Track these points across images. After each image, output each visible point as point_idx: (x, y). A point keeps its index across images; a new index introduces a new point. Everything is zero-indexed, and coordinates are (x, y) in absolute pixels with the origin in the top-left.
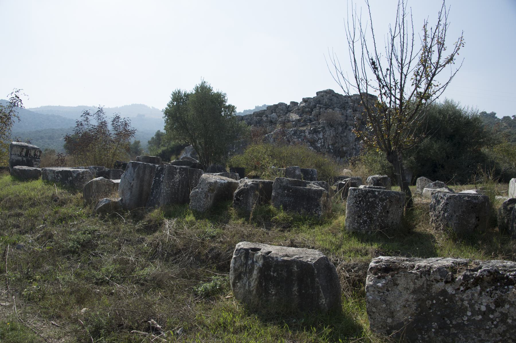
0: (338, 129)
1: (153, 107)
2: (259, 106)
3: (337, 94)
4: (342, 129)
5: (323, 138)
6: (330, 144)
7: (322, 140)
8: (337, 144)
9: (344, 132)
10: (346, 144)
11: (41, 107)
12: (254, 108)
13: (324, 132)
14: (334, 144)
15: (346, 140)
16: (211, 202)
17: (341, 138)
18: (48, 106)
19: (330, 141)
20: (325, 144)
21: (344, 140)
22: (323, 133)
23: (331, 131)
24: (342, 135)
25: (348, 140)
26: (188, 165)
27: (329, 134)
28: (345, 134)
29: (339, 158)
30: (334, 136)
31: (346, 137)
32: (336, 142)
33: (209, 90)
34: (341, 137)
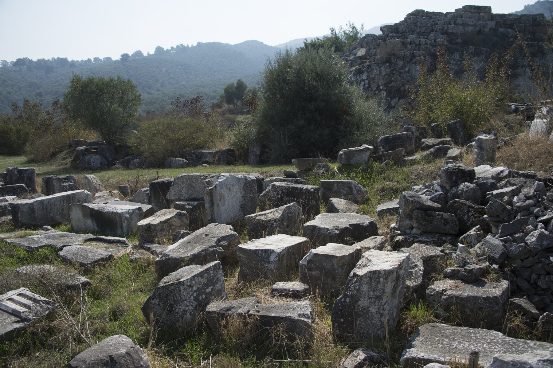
0: (395, 64)
1: (382, 29)
2: (530, 4)
3: (457, 10)
4: (404, 64)
5: (367, 79)
6: (380, 84)
7: (367, 82)
8: (393, 83)
9: (405, 67)
10: (408, 81)
11: (290, 41)
12: (523, 8)
13: (370, 72)
14: (389, 84)
15: (409, 77)
16: (169, 174)
17: (399, 75)
18: (296, 40)
19: (381, 81)
20: (372, 85)
21: (405, 77)
22: (368, 73)
23: (382, 68)
24: (402, 71)
25: (412, 75)
26: (97, 145)
27: (378, 73)
28: (407, 69)
29: (397, 99)
30: (387, 74)
31: (408, 72)
32: (392, 81)
33: (79, 80)
34: (400, 73)
